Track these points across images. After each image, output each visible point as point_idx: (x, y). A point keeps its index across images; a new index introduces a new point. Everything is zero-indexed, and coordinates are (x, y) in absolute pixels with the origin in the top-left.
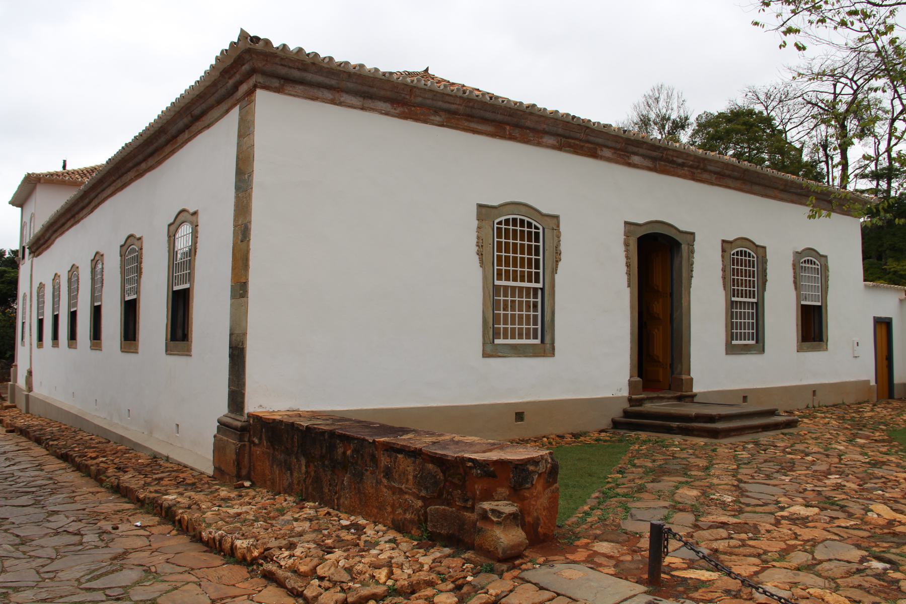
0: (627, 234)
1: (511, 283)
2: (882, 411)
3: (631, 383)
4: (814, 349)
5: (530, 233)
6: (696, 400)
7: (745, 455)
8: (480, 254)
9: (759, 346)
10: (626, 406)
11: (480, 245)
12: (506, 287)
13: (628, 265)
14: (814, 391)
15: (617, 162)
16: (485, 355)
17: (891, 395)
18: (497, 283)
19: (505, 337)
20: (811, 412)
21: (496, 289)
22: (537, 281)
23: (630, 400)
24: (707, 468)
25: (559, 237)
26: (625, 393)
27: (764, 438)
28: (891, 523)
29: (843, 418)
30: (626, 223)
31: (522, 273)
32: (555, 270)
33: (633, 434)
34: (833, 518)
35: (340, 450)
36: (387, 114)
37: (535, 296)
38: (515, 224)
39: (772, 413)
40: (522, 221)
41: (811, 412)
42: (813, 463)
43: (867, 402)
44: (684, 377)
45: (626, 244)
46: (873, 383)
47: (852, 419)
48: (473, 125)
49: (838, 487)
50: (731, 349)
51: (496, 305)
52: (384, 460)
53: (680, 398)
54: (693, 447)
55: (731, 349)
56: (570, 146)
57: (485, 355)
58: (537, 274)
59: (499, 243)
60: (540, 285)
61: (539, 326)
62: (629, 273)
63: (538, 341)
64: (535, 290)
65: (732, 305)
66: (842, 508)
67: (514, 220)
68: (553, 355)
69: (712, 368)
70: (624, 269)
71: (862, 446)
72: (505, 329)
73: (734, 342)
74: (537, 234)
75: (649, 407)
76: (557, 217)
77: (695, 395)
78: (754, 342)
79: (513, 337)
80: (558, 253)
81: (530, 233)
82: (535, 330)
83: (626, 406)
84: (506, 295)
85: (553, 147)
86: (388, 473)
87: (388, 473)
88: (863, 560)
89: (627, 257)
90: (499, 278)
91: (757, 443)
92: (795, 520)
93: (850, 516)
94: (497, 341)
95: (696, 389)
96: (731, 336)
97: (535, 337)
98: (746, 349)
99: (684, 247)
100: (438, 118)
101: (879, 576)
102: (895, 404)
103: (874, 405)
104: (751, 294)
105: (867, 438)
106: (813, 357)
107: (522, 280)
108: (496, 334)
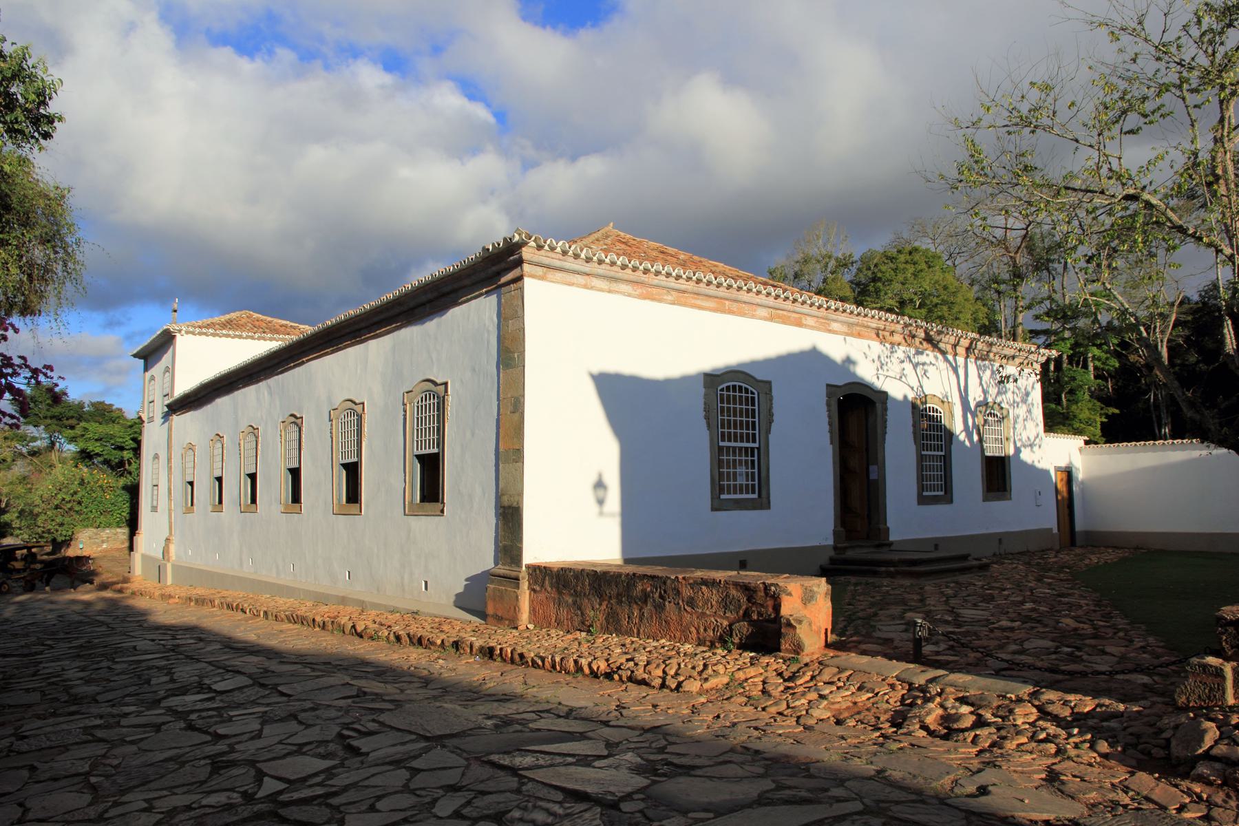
0: (829, 395)
1: (733, 444)
2: (1065, 557)
3: (835, 532)
4: (999, 499)
5: (747, 398)
6: (893, 548)
7: (949, 591)
8: (707, 418)
9: (947, 498)
10: (832, 553)
11: (707, 410)
12: (728, 448)
13: (830, 424)
14: (1000, 538)
15: (818, 329)
16: (714, 509)
17: (1073, 543)
18: (721, 444)
19: (729, 493)
20: (999, 558)
21: (721, 449)
22: (754, 441)
23: (835, 548)
24: (922, 601)
25: (771, 400)
26: (831, 542)
27: (963, 578)
28: (1076, 629)
29: (1029, 563)
30: (828, 385)
31: (735, 434)
32: (768, 431)
33: (842, 578)
34: (1033, 628)
35: (640, 587)
36: (629, 295)
37: (753, 455)
38: (734, 391)
39: (964, 558)
40: (740, 387)
41: (999, 558)
42: (1008, 596)
43: (1051, 549)
44: (881, 526)
45: (828, 405)
46: (1055, 531)
47: (1038, 564)
48: (699, 302)
49: (1033, 610)
50: (922, 500)
51: (720, 463)
52: (687, 592)
53: (878, 546)
54: (902, 586)
55: (922, 500)
56: (779, 317)
57: (714, 509)
58: (754, 435)
59: (722, 408)
60: (757, 445)
61: (756, 482)
62: (831, 432)
63: (755, 496)
64: (752, 449)
65: (921, 459)
66: (1039, 622)
67: (734, 387)
68: (768, 507)
69: (906, 518)
70: (827, 428)
71: (1049, 584)
72: (729, 486)
73: (925, 494)
74: (753, 399)
75: (850, 554)
76: (770, 383)
77: (891, 544)
78: (942, 493)
79: (735, 493)
80: (771, 415)
81: (747, 398)
82: (753, 486)
83: (832, 553)
84: (728, 454)
85: (765, 319)
86: (691, 602)
87: (691, 602)
88: (1057, 647)
89: (829, 417)
90: (723, 440)
91: (957, 583)
92: (1003, 629)
93: (1046, 626)
94: (723, 497)
95: (893, 537)
96: (921, 488)
97: (753, 492)
98: (935, 500)
99: (879, 406)
100: (670, 298)
101: (1071, 654)
102: (1078, 551)
103: (1058, 552)
104: (939, 448)
105: (1052, 578)
106: (997, 506)
107: (742, 441)
108: (721, 490)
